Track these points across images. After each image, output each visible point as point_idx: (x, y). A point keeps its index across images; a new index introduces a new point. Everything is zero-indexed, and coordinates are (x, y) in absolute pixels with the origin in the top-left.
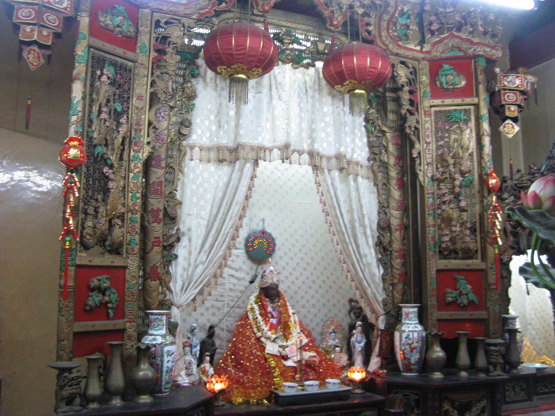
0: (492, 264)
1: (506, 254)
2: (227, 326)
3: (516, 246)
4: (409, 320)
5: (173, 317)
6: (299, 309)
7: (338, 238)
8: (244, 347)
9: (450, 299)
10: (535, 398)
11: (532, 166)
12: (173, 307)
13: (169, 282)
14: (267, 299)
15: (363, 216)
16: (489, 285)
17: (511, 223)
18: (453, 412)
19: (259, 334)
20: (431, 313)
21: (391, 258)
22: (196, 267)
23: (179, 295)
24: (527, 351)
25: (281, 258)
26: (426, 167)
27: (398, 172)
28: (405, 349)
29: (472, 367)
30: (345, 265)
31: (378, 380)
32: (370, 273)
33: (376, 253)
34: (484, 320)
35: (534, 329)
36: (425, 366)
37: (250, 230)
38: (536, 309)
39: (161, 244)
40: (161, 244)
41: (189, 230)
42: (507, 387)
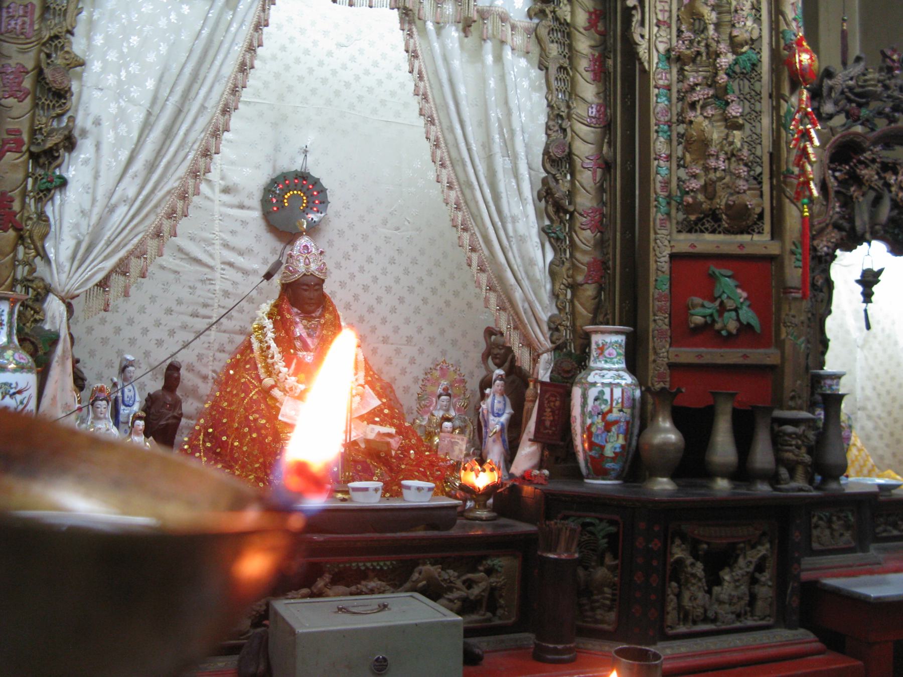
0: (794, 243)
1: (825, 239)
2: (214, 371)
3: (846, 225)
4: (606, 362)
5: (48, 319)
6: (376, 345)
7: (452, 175)
8: (233, 407)
9: (698, 320)
10: (873, 547)
11: (889, 53)
12: (51, 298)
13: (44, 236)
14: (296, 310)
15: (512, 132)
16: (787, 290)
17: (837, 174)
18: (693, 565)
19: (268, 381)
20: (654, 348)
21: (572, 228)
22: (112, 210)
23: (67, 269)
24: (856, 456)
25: (341, 233)
26: (655, 29)
27: (593, 43)
28: (591, 425)
29: (742, 473)
30: (466, 236)
31: (528, 489)
32: (522, 258)
33: (539, 216)
34: (772, 368)
35: (869, 417)
36: (637, 464)
37: (274, 170)
38: (877, 376)
39: (24, 148)
40: (24, 148)
41: (97, 123)
42: (815, 520)
